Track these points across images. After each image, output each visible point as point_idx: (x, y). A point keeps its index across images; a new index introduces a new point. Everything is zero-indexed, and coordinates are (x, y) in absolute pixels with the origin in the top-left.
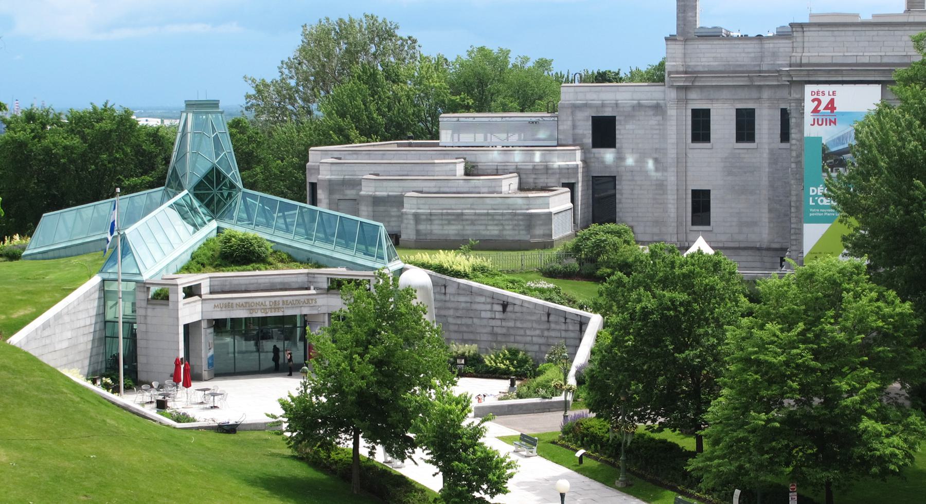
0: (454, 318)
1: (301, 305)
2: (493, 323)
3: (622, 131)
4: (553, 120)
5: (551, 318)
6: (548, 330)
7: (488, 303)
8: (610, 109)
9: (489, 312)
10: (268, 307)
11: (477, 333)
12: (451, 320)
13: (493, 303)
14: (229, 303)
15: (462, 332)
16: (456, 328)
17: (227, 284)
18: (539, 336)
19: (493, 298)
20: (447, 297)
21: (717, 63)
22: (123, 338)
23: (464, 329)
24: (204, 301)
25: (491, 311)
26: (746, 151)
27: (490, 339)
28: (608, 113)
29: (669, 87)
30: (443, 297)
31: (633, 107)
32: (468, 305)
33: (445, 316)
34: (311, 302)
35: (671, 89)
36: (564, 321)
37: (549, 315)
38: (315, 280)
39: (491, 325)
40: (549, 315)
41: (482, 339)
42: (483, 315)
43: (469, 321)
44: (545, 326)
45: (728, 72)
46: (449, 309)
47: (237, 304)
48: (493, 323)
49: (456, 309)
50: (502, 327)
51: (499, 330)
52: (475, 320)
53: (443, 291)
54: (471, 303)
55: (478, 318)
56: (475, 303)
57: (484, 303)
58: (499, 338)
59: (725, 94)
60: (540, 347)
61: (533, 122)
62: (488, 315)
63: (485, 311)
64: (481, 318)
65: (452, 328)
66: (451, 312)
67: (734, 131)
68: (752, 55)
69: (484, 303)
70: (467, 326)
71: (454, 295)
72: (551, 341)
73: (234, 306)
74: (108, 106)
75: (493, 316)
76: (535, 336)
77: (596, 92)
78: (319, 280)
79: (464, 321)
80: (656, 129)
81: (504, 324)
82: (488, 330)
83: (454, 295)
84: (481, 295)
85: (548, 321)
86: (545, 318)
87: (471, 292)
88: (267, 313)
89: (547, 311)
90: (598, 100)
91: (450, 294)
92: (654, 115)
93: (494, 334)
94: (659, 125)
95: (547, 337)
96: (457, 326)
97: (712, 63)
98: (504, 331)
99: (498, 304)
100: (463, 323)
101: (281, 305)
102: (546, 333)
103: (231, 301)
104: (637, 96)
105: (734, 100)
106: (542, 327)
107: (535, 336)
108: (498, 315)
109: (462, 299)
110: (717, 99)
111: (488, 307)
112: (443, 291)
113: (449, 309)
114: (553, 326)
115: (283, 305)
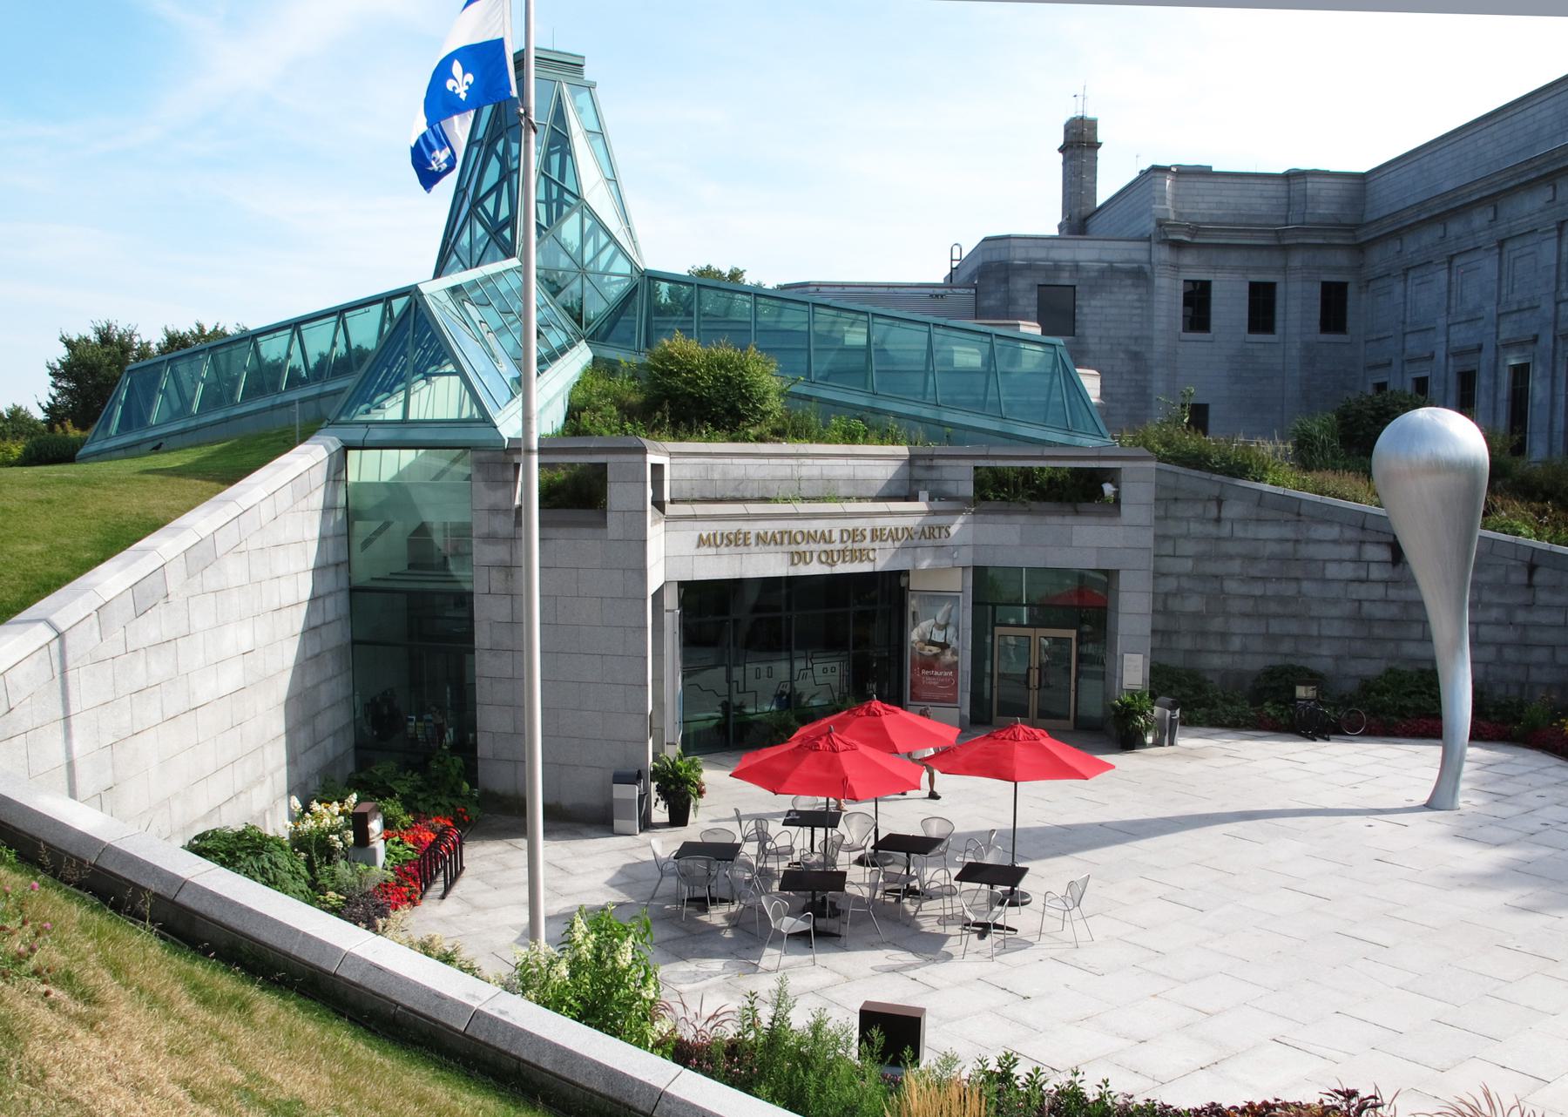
0: (1242, 580)
1: (916, 541)
2: (1361, 591)
3: (1086, 310)
4: (969, 294)
5: (1539, 578)
6: (1529, 606)
7: (1349, 542)
8: (1066, 274)
9: (1351, 566)
10: (838, 546)
11: (1312, 618)
12: (1232, 586)
13: (1362, 542)
14: (739, 532)
15: (1268, 616)
16: (1248, 606)
17: (716, 476)
18: (1498, 623)
19: (1363, 528)
20: (1225, 530)
21: (1220, 212)
22: (522, 651)
23: (1273, 607)
24: (671, 524)
25: (1358, 560)
26: (1262, 346)
27: (1348, 632)
28: (1065, 279)
29: (1158, 243)
30: (1211, 529)
31: (1102, 272)
32: (1289, 547)
33: (1216, 577)
34: (936, 533)
35: (1160, 246)
36: (1524, 579)
37: (1532, 569)
38: (935, 474)
39: (1354, 597)
40: (1532, 569)
41: (1326, 632)
42: (1332, 571)
43: (1290, 589)
44: (1522, 598)
45: (1240, 225)
46: (1231, 557)
47: (758, 536)
48: (1361, 591)
49: (1252, 559)
50: (1386, 601)
51: (1378, 611)
52: (1307, 586)
53: (1213, 512)
54: (1297, 541)
55: (1316, 580)
56: (1309, 541)
57: (1335, 542)
58: (1378, 631)
59: (1234, 258)
60: (1554, 654)
61: (937, 296)
62: (1349, 571)
63: (1341, 561)
64: (1325, 580)
65: (1235, 606)
66: (1235, 566)
67: (1246, 316)
68: (1274, 201)
69: (1335, 542)
70: (1282, 600)
71: (1245, 521)
72: (1534, 635)
73: (753, 540)
74: (219, 329)
75: (1363, 574)
76: (1487, 623)
77: (1045, 247)
78: (946, 474)
79: (1271, 588)
80: (1137, 308)
81: (1393, 593)
82: (1347, 609)
83: (1245, 521)
84: (1330, 522)
85: (1530, 585)
86: (1519, 577)
87: (1299, 514)
88: (833, 564)
89: (1528, 559)
90: (1048, 261)
91: (1233, 521)
92: (1133, 285)
93: (1359, 619)
94: (1140, 300)
95: (1525, 626)
96: (1251, 603)
97: (1215, 212)
98: (1393, 611)
99: (1378, 543)
100: (1269, 593)
101: (867, 543)
102: (1521, 616)
103: (745, 526)
104: (1107, 256)
105: (1248, 269)
106: (1508, 600)
107: (1487, 623)
108: (1376, 572)
109: (1268, 532)
110: (1223, 268)
111: (1349, 551)
112: (1213, 512)
113: (1231, 557)
114: (1543, 597)
115: (873, 540)
